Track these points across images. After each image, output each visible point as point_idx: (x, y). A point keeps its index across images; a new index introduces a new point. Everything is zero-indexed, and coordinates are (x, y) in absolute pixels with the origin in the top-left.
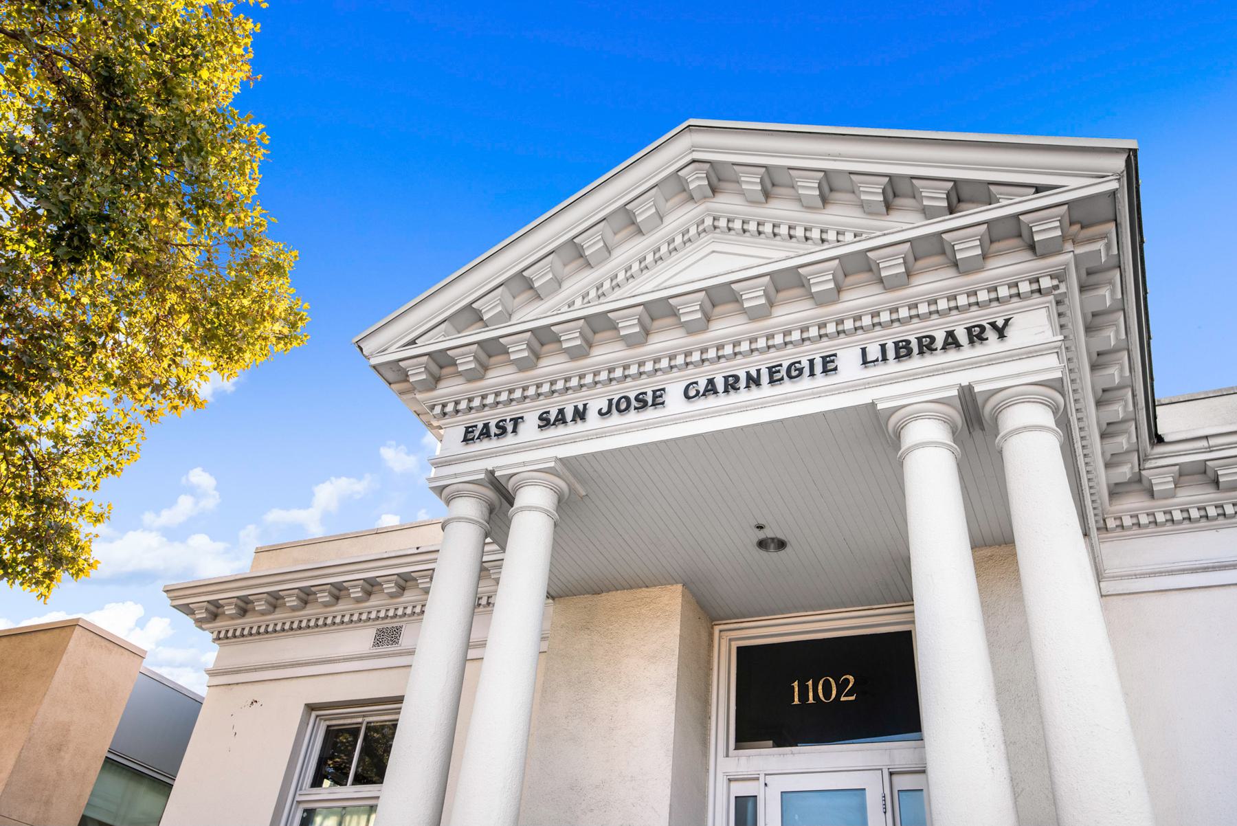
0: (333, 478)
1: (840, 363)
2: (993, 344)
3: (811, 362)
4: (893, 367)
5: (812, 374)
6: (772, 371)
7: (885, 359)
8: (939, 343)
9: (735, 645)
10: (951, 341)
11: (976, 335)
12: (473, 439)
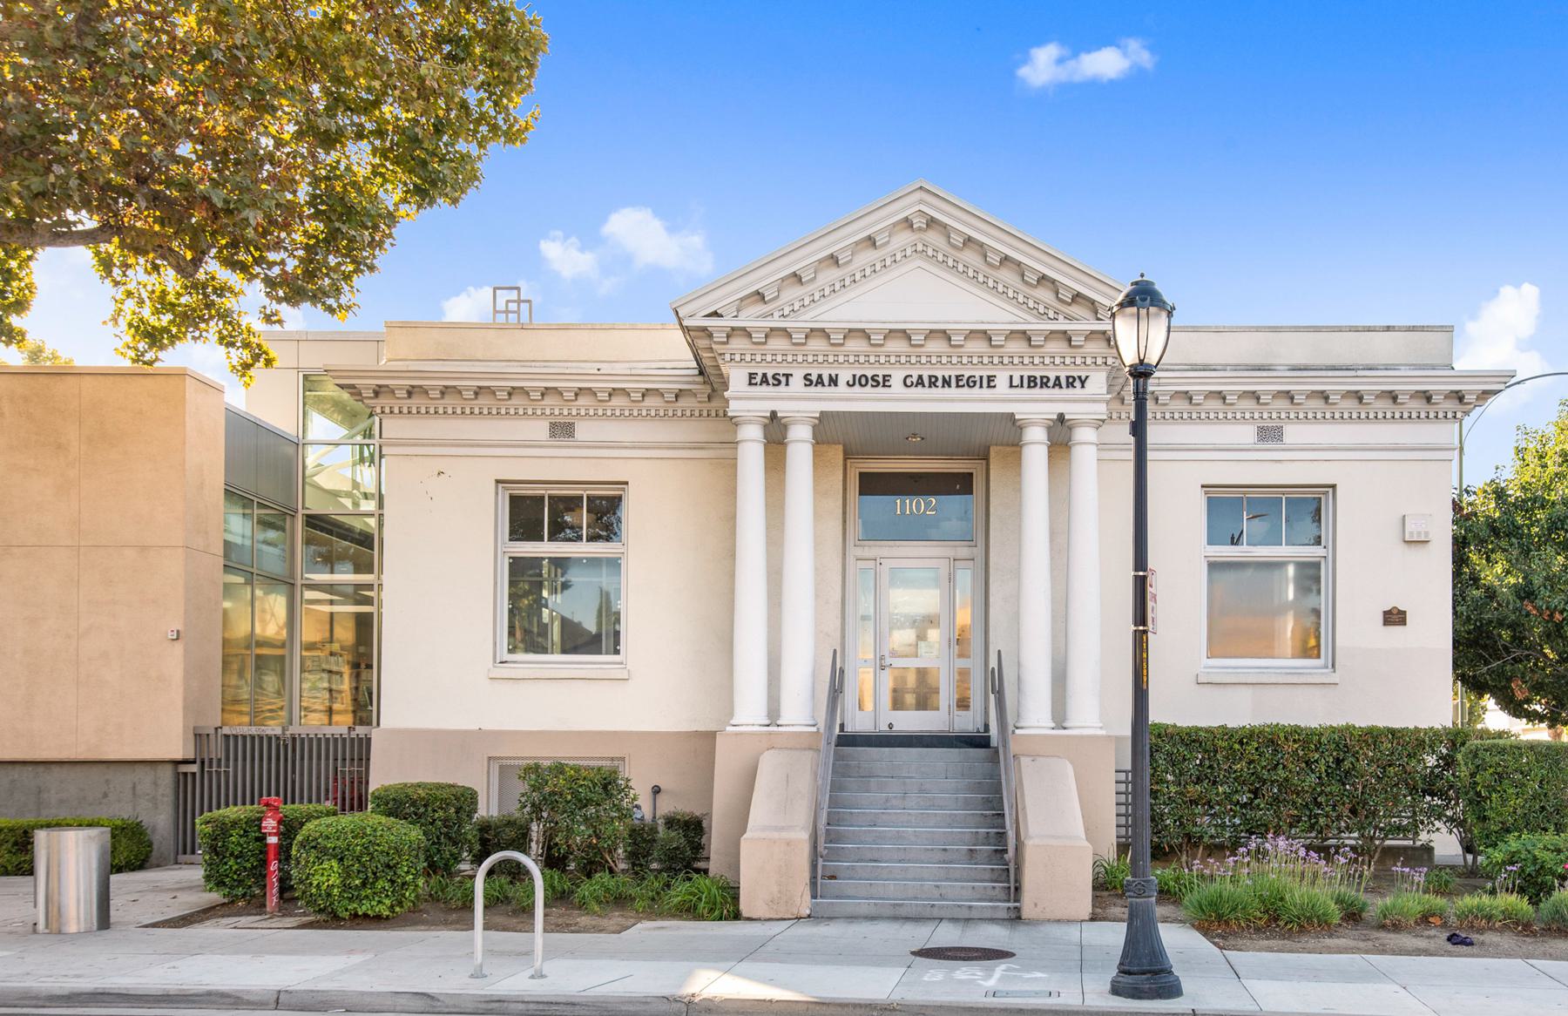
0: (471, 289)
1: (997, 382)
2: (1077, 391)
3: (981, 377)
4: (1025, 390)
5: (981, 387)
6: (958, 378)
7: (1022, 386)
8: (1051, 384)
9: (858, 471)
10: (1057, 383)
11: (1070, 383)
12: (756, 384)
